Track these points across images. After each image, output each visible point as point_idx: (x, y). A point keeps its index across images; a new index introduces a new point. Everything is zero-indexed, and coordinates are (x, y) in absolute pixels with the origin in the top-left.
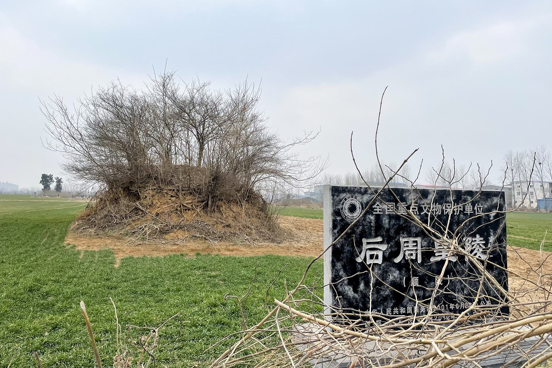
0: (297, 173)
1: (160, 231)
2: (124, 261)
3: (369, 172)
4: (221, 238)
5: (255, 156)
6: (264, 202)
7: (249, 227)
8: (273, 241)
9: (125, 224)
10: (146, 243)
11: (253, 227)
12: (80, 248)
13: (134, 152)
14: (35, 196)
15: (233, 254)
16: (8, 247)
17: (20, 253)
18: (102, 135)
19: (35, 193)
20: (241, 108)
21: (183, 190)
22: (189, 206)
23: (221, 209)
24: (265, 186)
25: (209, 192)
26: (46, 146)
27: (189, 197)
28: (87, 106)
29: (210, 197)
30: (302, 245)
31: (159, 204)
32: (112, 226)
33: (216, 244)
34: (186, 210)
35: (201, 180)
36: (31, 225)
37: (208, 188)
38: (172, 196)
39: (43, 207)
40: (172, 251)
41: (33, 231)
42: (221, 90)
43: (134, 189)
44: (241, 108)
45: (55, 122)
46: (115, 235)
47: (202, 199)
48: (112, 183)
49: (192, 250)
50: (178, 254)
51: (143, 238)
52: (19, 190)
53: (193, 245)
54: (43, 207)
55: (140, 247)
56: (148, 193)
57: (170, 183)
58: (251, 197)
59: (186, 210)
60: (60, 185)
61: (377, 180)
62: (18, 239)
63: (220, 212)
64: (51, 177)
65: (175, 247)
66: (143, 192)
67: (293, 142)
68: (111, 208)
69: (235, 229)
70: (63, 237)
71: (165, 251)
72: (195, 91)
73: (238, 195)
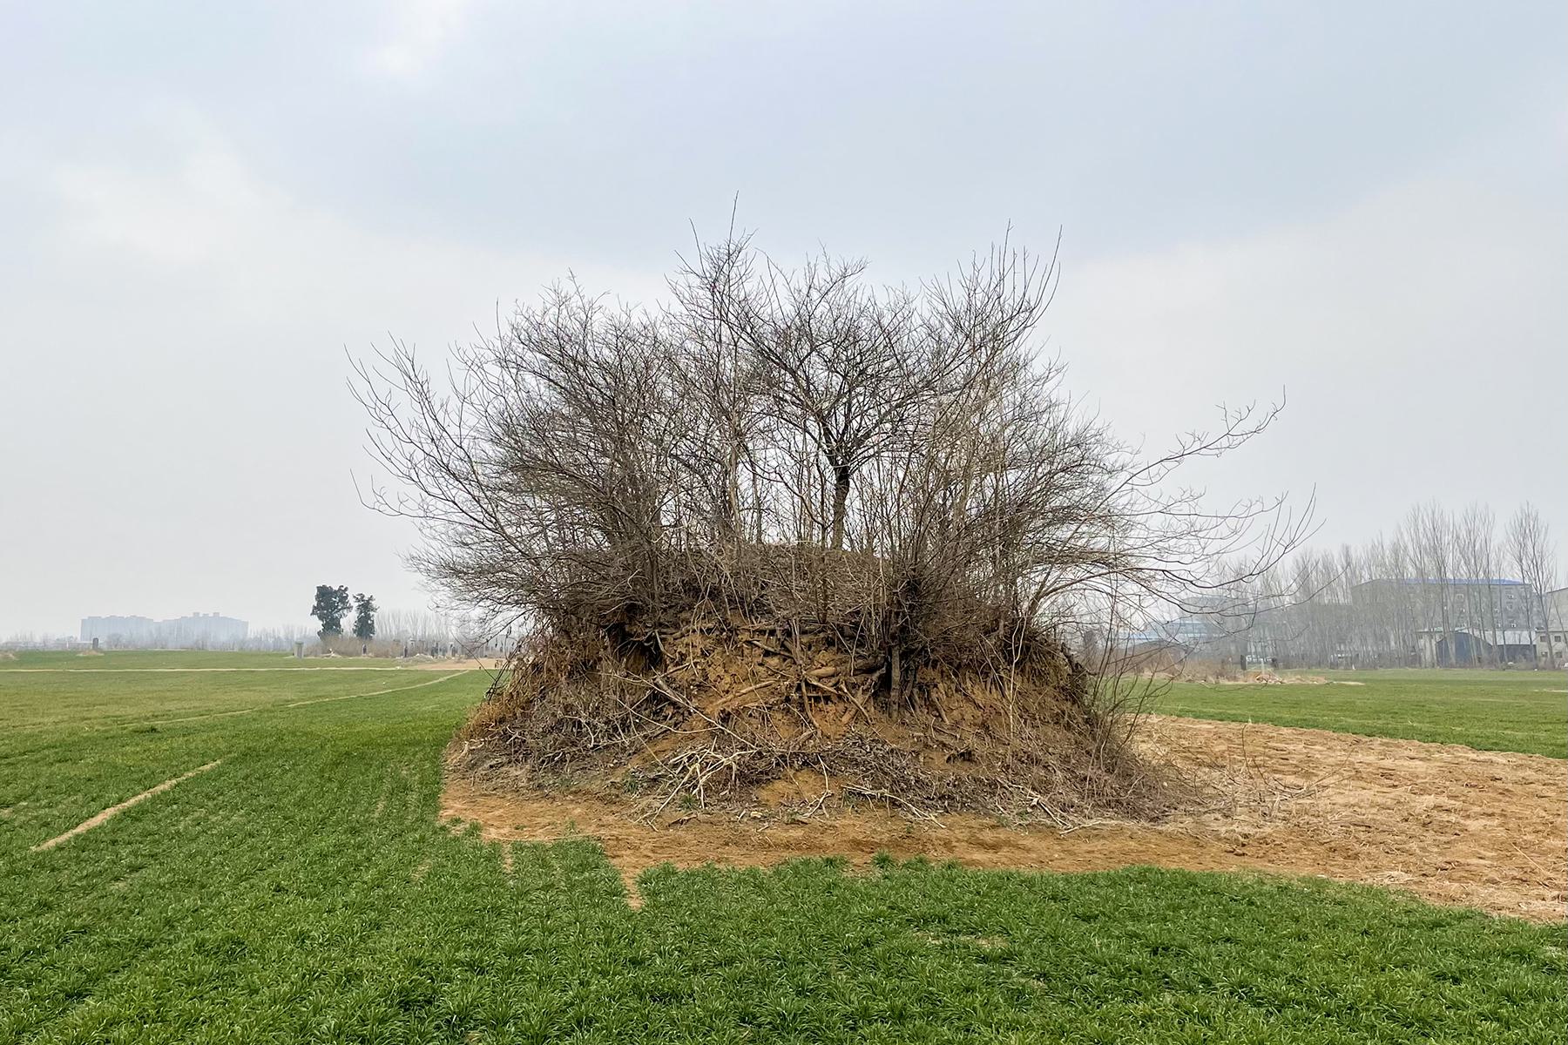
0: (1187, 559)
1: (741, 775)
2: (657, 883)
3: (1387, 544)
4: (947, 801)
5: (1030, 505)
6: (1076, 668)
7: (1038, 762)
8: (1134, 813)
9: (624, 749)
10: (701, 816)
11: (1052, 761)
12: (493, 834)
13: (622, 506)
14: (299, 653)
15: (998, 862)
16: (278, 832)
17: (323, 856)
18: (530, 459)
19: (300, 645)
20: (987, 338)
21: (803, 633)
22: (828, 687)
23: (934, 696)
24: (1076, 607)
25: (893, 637)
26: (371, 500)
27: (824, 656)
28: (475, 366)
29: (896, 653)
30: (1247, 830)
31: (728, 679)
32: (582, 759)
33: (933, 823)
34: (817, 699)
35: (863, 596)
36: (327, 755)
37: (885, 623)
38: (767, 654)
39: (331, 688)
40: (787, 847)
41: (338, 774)
42: (904, 284)
43: (641, 630)
44: (987, 338)
45: (392, 423)
46: (595, 787)
47: (871, 660)
48: (566, 612)
49: (857, 844)
50: (816, 857)
51: (687, 800)
52: (251, 635)
53: (854, 824)
54: (331, 688)
55: (681, 832)
56: (690, 642)
57: (760, 608)
58: (1028, 650)
59: (817, 699)
60: (368, 617)
61: (1421, 572)
62: (301, 803)
63: (931, 705)
64: (342, 594)
65: (797, 833)
66: (671, 639)
67: (1178, 449)
68: (568, 693)
69: (990, 766)
70: (434, 796)
71: (766, 846)
72: (815, 295)
73: (990, 643)
